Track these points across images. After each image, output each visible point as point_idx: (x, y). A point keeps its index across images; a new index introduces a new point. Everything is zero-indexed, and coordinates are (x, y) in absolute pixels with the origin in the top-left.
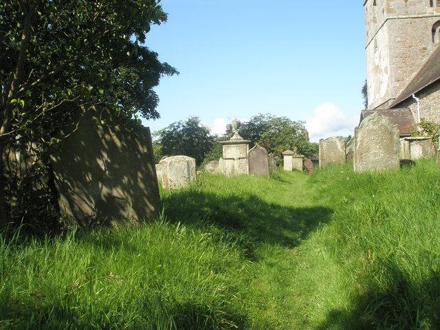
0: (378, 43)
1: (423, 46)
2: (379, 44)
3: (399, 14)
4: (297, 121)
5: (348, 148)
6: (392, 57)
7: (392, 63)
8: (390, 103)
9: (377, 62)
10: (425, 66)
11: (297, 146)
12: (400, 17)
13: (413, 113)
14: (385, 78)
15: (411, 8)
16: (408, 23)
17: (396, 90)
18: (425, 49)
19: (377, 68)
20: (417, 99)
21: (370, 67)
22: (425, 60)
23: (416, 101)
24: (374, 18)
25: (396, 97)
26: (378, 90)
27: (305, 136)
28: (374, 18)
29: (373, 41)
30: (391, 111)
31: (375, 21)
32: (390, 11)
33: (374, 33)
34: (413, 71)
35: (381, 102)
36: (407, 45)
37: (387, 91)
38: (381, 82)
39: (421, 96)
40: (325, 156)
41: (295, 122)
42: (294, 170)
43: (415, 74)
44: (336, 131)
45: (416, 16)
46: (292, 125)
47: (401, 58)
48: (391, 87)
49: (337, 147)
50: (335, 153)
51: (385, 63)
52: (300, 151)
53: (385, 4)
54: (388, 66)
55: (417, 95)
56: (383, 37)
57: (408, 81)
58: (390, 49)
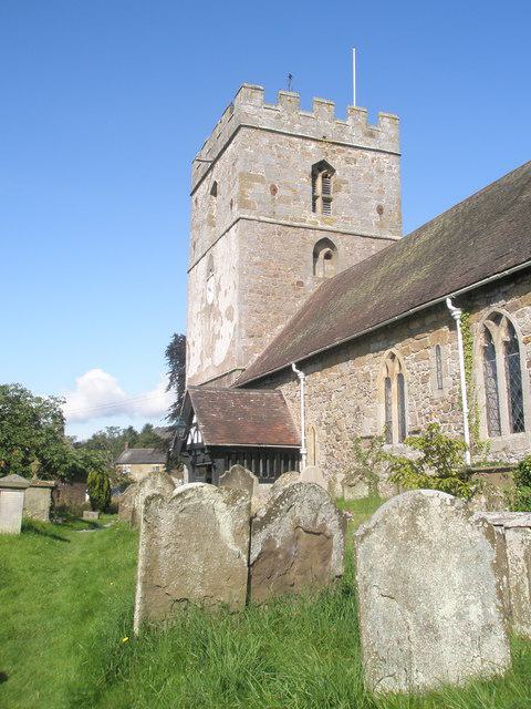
0: (215, 262)
1: (298, 278)
2: (218, 263)
3: (260, 213)
4: (45, 398)
5: (261, 536)
6: (243, 290)
7: (242, 301)
8: (235, 378)
9: (211, 297)
10: (300, 315)
11: (41, 457)
12: (262, 218)
13: (288, 401)
14: (227, 329)
15: (281, 208)
16: (274, 233)
17: (248, 352)
18: (300, 284)
19: (210, 310)
20: (301, 375)
21: (196, 307)
22: (300, 303)
23: (296, 378)
24: (211, 217)
25: (247, 367)
26: (209, 350)
27: (56, 434)
28: (211, 217)
29: (205, 259)
30: (247, 393)
31: (212, 224)
32: (244, 204)
33: (208, 244)
34: (278, 321)
35: (214, 374)
36: (271, 272)
37: (229, 353)
38: (218, 336)
39: (310, 368)
40: (164, 568)
41: (39, 400)
42: (28, 527)
43: (281, 328)
44: (109, 415)
45: (288, 223)
46: (34, 405)
47: (259, 294)
48: (239, 345)
49: (216, 534)
50: (207, 559)
51: (228, 300)
52: (47, 470)
53: (235, 192)
54: (235, 307)
55: (301, 365)
56: (228, 252)
57: (269, 339)
58: (241, 273)
